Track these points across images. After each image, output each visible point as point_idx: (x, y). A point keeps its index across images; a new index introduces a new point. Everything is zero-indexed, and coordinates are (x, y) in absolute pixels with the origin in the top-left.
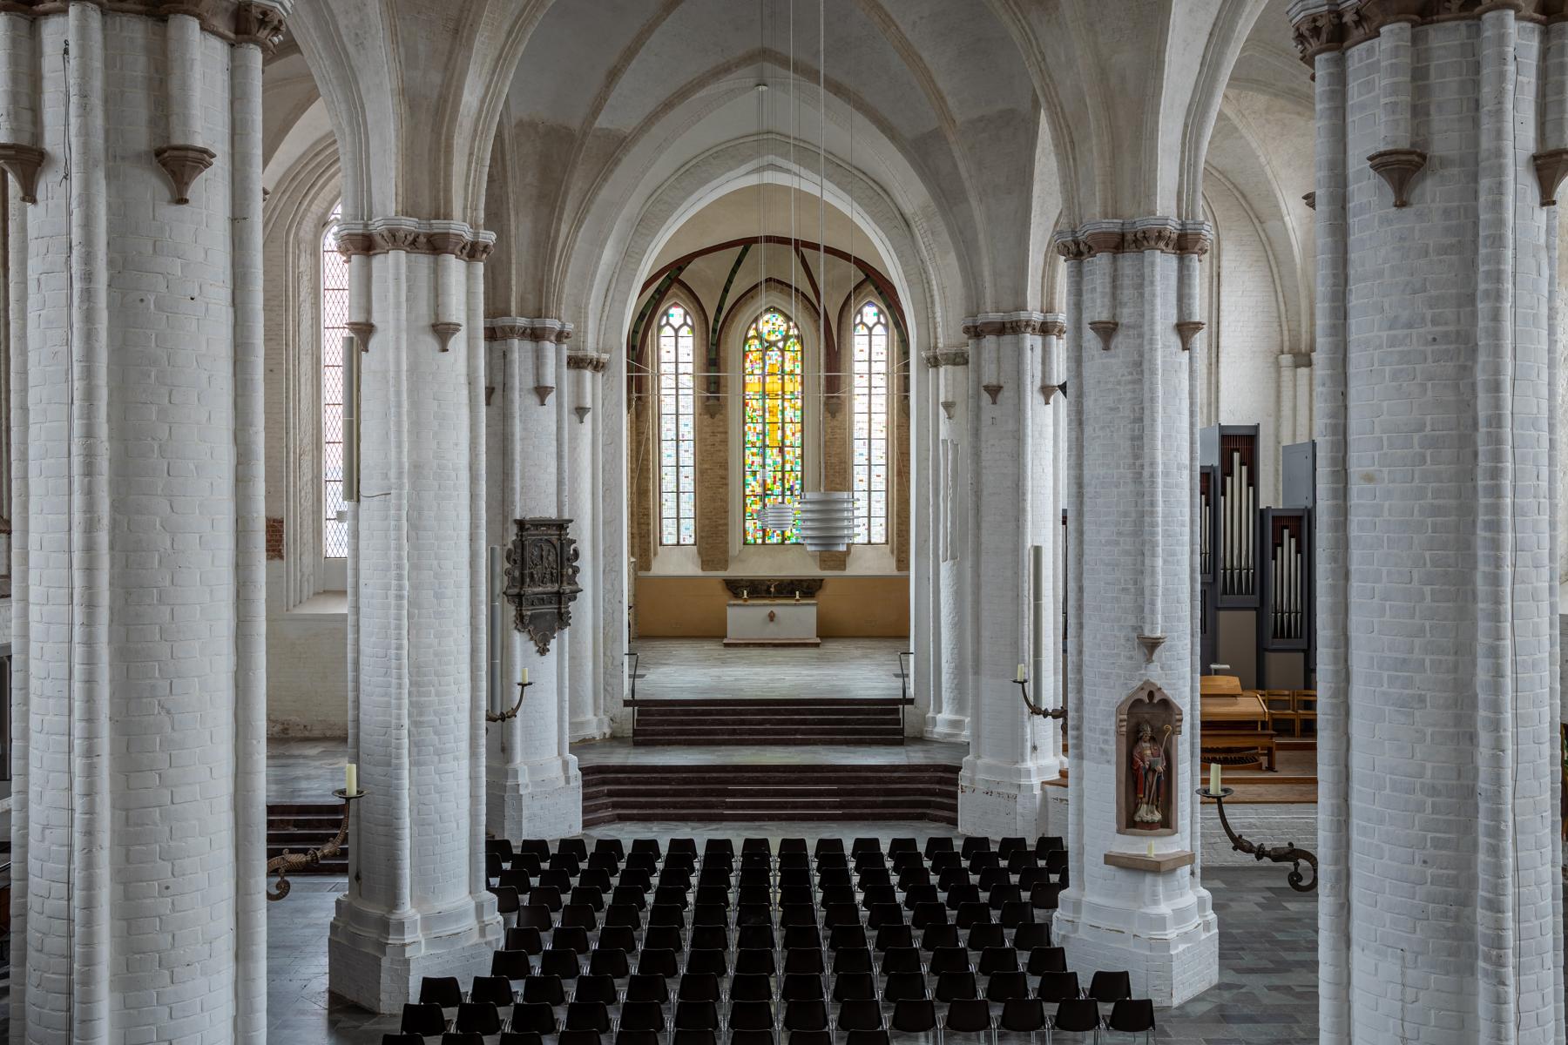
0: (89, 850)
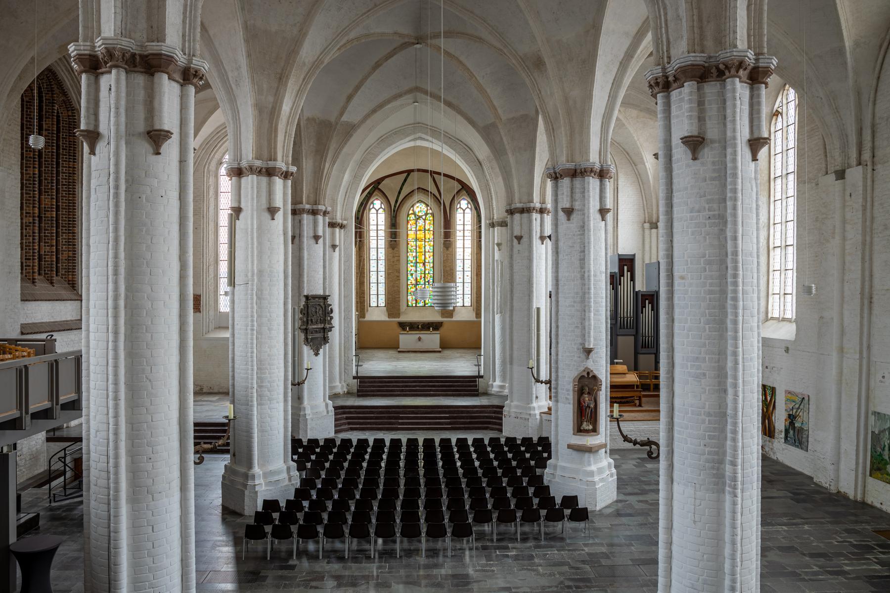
0: (116, 442)
